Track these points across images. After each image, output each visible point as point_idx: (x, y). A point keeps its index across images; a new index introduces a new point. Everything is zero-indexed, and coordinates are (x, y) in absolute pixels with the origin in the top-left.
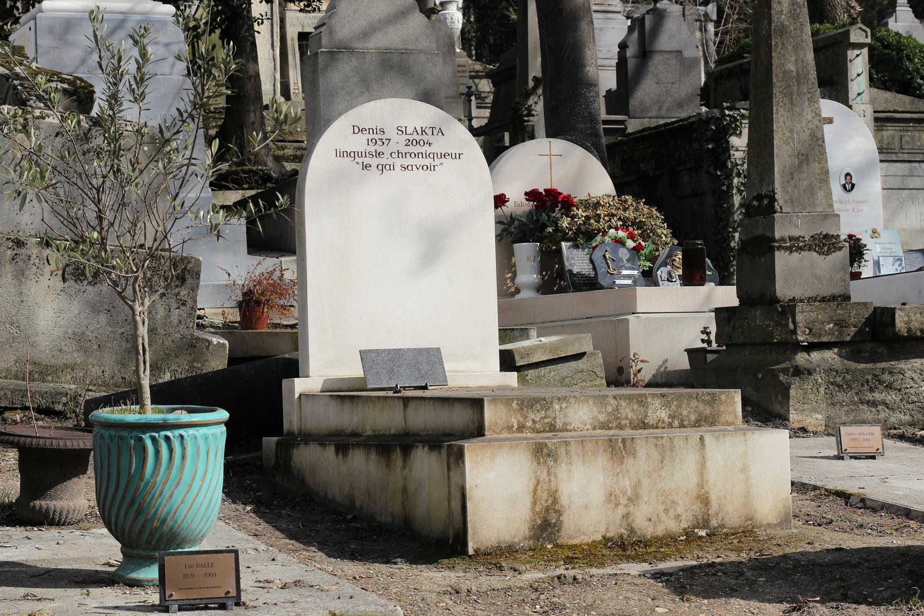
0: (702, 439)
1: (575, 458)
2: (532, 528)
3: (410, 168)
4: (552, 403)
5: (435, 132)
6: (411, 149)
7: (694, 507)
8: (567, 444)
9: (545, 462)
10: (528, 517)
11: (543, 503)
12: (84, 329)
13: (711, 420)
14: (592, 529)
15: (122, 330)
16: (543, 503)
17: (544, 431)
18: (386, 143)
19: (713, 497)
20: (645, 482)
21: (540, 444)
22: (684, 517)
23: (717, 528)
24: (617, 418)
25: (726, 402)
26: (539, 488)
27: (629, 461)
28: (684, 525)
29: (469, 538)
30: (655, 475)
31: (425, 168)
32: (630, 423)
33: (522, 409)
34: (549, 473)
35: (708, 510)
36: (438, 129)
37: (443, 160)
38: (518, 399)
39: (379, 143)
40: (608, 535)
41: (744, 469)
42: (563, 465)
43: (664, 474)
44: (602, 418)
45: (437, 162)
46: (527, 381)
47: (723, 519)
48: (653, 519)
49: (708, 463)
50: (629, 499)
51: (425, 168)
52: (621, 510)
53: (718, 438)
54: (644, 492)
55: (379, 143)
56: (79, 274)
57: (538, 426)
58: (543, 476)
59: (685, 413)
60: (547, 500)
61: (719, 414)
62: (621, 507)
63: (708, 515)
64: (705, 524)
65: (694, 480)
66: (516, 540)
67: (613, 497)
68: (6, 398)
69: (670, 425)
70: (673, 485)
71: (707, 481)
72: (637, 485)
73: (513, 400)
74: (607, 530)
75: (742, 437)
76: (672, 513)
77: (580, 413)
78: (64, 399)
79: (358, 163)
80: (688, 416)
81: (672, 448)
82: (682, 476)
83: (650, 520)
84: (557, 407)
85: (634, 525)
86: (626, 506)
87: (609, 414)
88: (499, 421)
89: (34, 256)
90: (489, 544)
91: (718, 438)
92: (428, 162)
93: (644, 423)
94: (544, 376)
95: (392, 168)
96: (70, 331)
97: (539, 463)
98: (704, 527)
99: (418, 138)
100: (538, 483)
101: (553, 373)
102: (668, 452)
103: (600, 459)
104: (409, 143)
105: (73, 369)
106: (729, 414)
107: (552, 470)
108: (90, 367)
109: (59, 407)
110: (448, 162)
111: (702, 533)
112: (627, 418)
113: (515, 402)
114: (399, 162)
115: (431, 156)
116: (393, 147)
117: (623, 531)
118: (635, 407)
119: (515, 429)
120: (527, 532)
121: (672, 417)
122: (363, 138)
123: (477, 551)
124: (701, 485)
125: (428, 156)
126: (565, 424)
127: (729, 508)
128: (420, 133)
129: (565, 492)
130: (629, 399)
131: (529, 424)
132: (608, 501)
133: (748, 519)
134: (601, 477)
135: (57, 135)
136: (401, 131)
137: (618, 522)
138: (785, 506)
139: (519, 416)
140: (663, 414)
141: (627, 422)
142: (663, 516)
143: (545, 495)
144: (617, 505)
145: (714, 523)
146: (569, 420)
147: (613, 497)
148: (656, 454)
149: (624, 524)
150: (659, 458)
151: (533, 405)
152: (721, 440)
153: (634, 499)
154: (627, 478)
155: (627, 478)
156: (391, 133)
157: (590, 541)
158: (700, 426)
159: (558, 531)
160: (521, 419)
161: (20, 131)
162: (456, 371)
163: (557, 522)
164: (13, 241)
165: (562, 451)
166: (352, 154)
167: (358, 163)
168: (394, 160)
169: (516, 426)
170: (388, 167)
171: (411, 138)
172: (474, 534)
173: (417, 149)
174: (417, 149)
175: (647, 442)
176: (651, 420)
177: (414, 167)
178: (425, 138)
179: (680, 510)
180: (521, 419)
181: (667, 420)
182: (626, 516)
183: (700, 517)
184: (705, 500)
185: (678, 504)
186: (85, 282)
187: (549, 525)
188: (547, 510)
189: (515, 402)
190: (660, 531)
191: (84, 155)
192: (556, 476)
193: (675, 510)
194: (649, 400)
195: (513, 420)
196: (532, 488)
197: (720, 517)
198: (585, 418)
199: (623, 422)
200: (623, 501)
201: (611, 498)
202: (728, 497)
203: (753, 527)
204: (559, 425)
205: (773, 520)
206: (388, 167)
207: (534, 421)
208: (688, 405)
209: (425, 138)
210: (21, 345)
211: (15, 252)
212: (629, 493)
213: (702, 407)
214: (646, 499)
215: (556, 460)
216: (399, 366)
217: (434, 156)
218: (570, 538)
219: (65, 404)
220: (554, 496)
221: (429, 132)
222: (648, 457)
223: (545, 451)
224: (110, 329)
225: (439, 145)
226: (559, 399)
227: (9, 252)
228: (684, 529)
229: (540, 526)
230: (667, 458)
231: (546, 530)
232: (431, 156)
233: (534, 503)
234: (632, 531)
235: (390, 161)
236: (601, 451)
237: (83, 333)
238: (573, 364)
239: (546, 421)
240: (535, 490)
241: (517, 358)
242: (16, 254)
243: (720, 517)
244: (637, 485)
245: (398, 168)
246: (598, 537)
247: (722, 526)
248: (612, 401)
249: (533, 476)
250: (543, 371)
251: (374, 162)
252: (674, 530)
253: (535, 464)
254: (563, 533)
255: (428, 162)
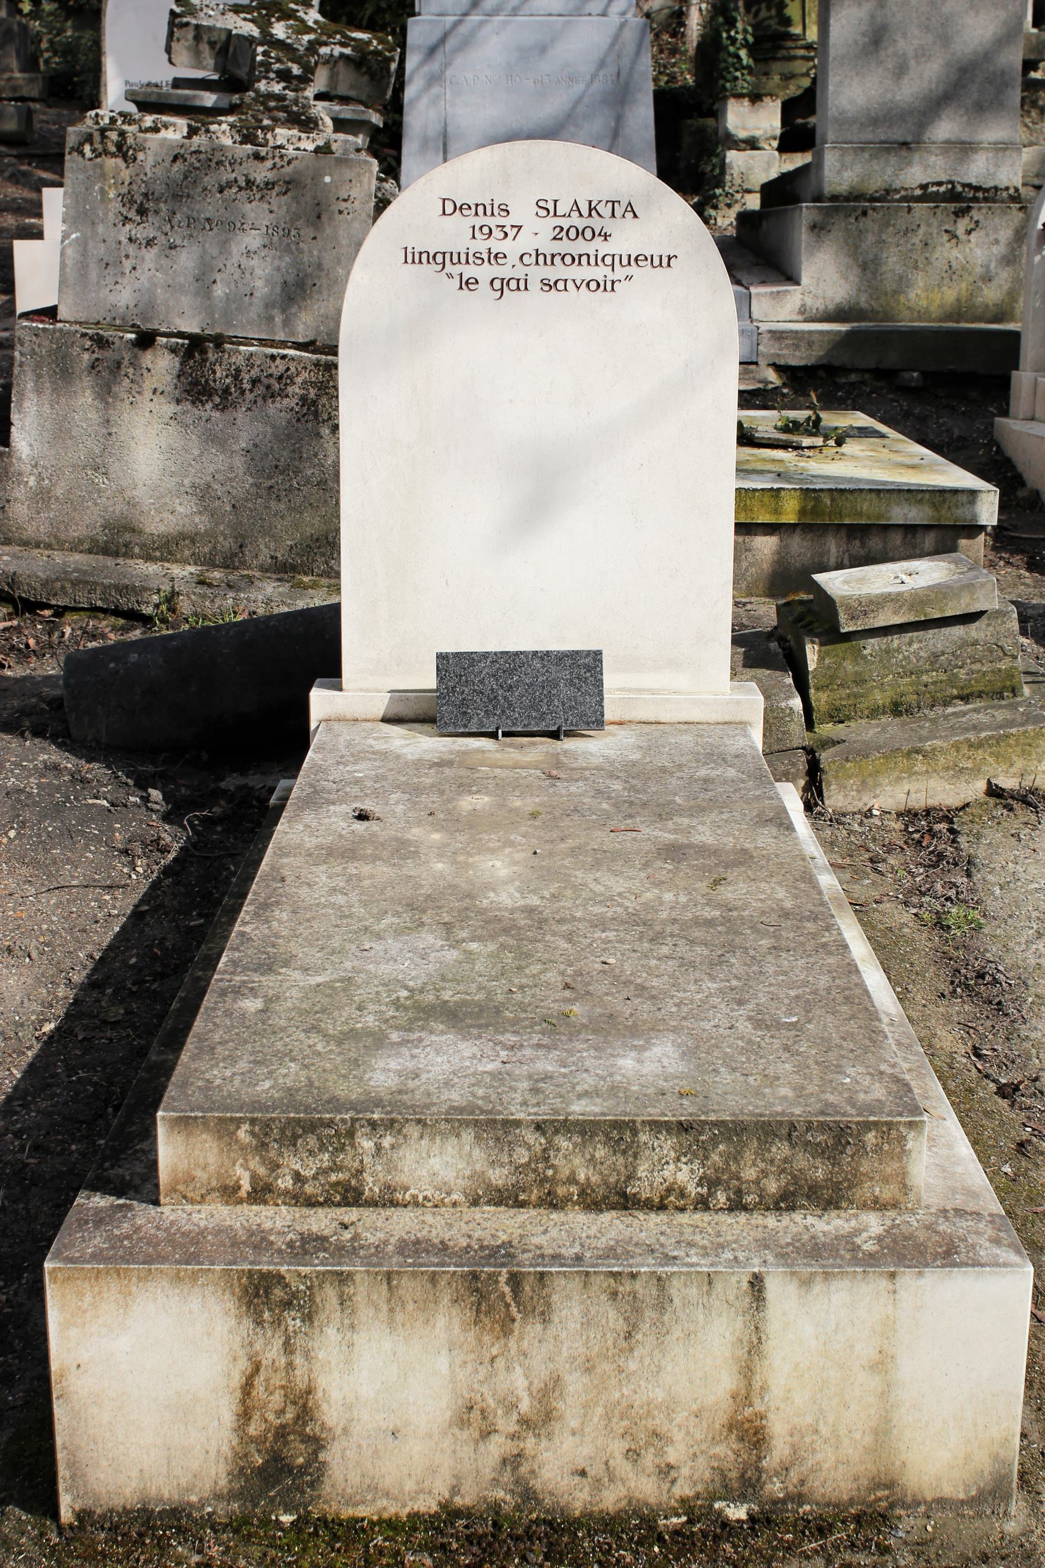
0: (757, 1283)
1: (365, 1313)
2: (239, 1473)
3: (561, 285)
4: (351, 1134)
5: (618, 212)
6: (564, 246)
7: (720, 1450)
8: (343, 1279)
9: (277, 1322)
10: (226, 1449)
11: (271, 1417)
12: (209, 478)
13: (826, 1194)
14: (410, 1486)
15: (270, 483)
16: (271, 1417)
17: (328, 1203)
18: (512, 233)
19: (778, 1429)
20: (575, 1383)
21: (265, 1276)
22: (685, 1471)
23: (784, 1501)
24: (545, 1179)
25: (878, 1149)
26: (259, 1381)
27: (529, 1333)
28: (683, 1489)
29: (61, 1486)
30: (606, 1367)
31: (593, 286)
32: (582, 1193)
33: (264, 1145)
34: (288, 1348)
35: (760, 1459)
36: (624, 204)
37: (633, 270)
38: (253, 1121)
39: (497, 234)
40: (458, 1501)
41: (882, 1364)
42: (331, 1332)
43: (632, 1366)
44: (499, 1176)
45: (620, 273)
46: (864, 657)
47: (802, 1482)
48: (591, 1472)
49: (769, 1346)
50: (525, 1422)
51: (593, 286)
52: (497, 1447)
53: (806, 1283)
54: (568, 1412)
55: (497, 234)
56: (199, 393)
57: (309, 1189)
58: (272, 1353)
59: (750, 1173)
60: (281, 1412)
61: (855, 1180)
62: (495, 1438)
63: (759, 1470)
64: (747, 1485)
65: (725, 1383)
66: (194, 1498)
67: (476, 1414)
68: (65, 594)
69: (703, 1204)
70: (659, 1395)
71: (764, 1389)
72: (549, 1391)
73: (239, 1122)
74: (455, 1490)
75: (884, 1283)
76: (649, 1459)
77: (435, 1163)
78: (155, 598)
79: (450, 276)
80: (757, 1182)
81: (663, 1302)
82: (689, 1373)
83: (583, 1473)
84: (367, 1144)
85: (536, 1484)
86: (513, 1437)
87: (518, 1169)
88: (198, 1173)
89: (126, 362)
90: (118, 1503)
91: (806, 1283)
92: (599, 273)
93: (624, 1195)
94: (898, 650)
95: (522, 285)
96: (186, 482)
97: (259, 1323)
98: (743, 1498)
99: (580, 223)
100: (257, 1368)
101: (915, 646)
102: (649, 1314)
103: (441, 1321)
104: (560, 234)
105: (193, 542)
106: (886, 1180)
107: (299, 1341)
108: (221, 539)
109: (148, 610)
110: (642, 273)
111: (737, 1512)
112: (572, 1180)
113: (246, 1127)
114: (537, 273)
115: (608, 260)
116: (526, 243)
117: (501, 1494)
118: (601, 1152)
119: (243, 1193)
120: (223, 1482)
121: (711, 1183)
122: (461, 224)
123: (83, 1516)
124: (744, 1397)
125: (599, 260)
126: (388, 1187)
127: (826, 1456)
128: (585, 212)
129: (335, 1395)
130: (583, 1133)
131: (285, 1182)
132: (462, 1422)
133: (877, 1484)
134: (443, 1363)
135: (175, 158)
136: (547, 208)
137: (488, 1474)
138: (996, 1458)
139: (255, 1163)
140: (685, 1176)
141: (574, 1189)
142: (622, 1466)
143: (277, 1400)
144: (486, 1434)
145: (775, 1488)
146: (403, 1178)
147: (476, 1414)
148: (612, 1314)
149: (507, 1477)
150: (621, 1325)
151: (295, 1137)
152: (818, 1288)
153: (540, 1421)
154: (519, 1371)
155: (519, 1371)
156: (522, 212)
157: (404, 1513)
158: (792, 1208)
159: (312, 1485)
160: (262, 1171)
161: (113, 155)
162: (639, 690)
163: (308, 1464)
164: (91, 338)
165: (330, 1294)
166: (439, 258)
167: (450, 276)
168: (527, 270)
169: (246, 1186)
170: (513, 284)
171: (565, 223)
172: (73, 1477)
173: (580, 247)
174: (580, 247)
175: (585, 1285)
176: (643, 1188)
177: (570, 284)
178: (596, 223)
179: (673, 1455)
180: (262, 1171)
181: (692, 1189)
182: (513, 1461)
183: (734, 1474)
184: (751, 1434)
185: (670, 1441)
186: (209, 406)
187: (289, 1470)
188: (281, 1433)
189: (246, 1127)
190: (611, 1500)
191: (221, 192)
192: (307, 1355)
193: (660, 1453)
194: (643, 1137)
195: (239, 1171)
196: (237, 1379)
197: (794, 1476)
198: (449, 1175)
199: (561, 1191)
200: (507, 1424)
201: (472, 1418)
202: (825, 1431)
203: (892, 1506)
204: (371, 1186)
205: (953, 1489)
206: (513, 284)
207: (298, 1177)
208: (761, 1152)
209: (596, 223)
210: (111, 502)
211: (96, 356)
212: (525, 1406)
213: (802, 1161)
214: (574, 1423)
215: (308, 1318)
216: (510, 688)
217: (614, 261)
218: (351, 1502)
219: (157, 606)
220: (303, 1403)
221: (606, 211)
222: (588, 1322)
223: (278, 1293)
224: (251, 481)
225: (627, 238)
226: (373, 1125)
227: (86, 356)
228: (683, 1501)
229: (261, 1471)
230: (645, 1327)
231: (278, 1482)
232: (608, 260)
233: (245, 1415)
234: (528, 1496)
235: (520, 272)
236: (446, 1300)
237: (209, 486)
238: (958, 631)
239: (333, 1177)
240: (247, 1387)
241: (842, 617)
242: (97, 359)
243: (794, 1476)
244: (549, 1391)
245: (535, 285)
246: (428, 1505)
247: (800, 1498)
248: (531, 1137)
249: (241, 1353)
250: (895, 641)
251: (484, 273)
252: (652, 1500)
253: (248, 1323)
254: (326, 1489)
255: (599, 273)
